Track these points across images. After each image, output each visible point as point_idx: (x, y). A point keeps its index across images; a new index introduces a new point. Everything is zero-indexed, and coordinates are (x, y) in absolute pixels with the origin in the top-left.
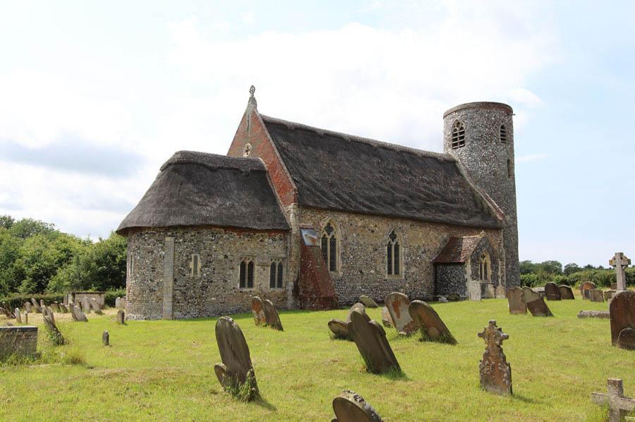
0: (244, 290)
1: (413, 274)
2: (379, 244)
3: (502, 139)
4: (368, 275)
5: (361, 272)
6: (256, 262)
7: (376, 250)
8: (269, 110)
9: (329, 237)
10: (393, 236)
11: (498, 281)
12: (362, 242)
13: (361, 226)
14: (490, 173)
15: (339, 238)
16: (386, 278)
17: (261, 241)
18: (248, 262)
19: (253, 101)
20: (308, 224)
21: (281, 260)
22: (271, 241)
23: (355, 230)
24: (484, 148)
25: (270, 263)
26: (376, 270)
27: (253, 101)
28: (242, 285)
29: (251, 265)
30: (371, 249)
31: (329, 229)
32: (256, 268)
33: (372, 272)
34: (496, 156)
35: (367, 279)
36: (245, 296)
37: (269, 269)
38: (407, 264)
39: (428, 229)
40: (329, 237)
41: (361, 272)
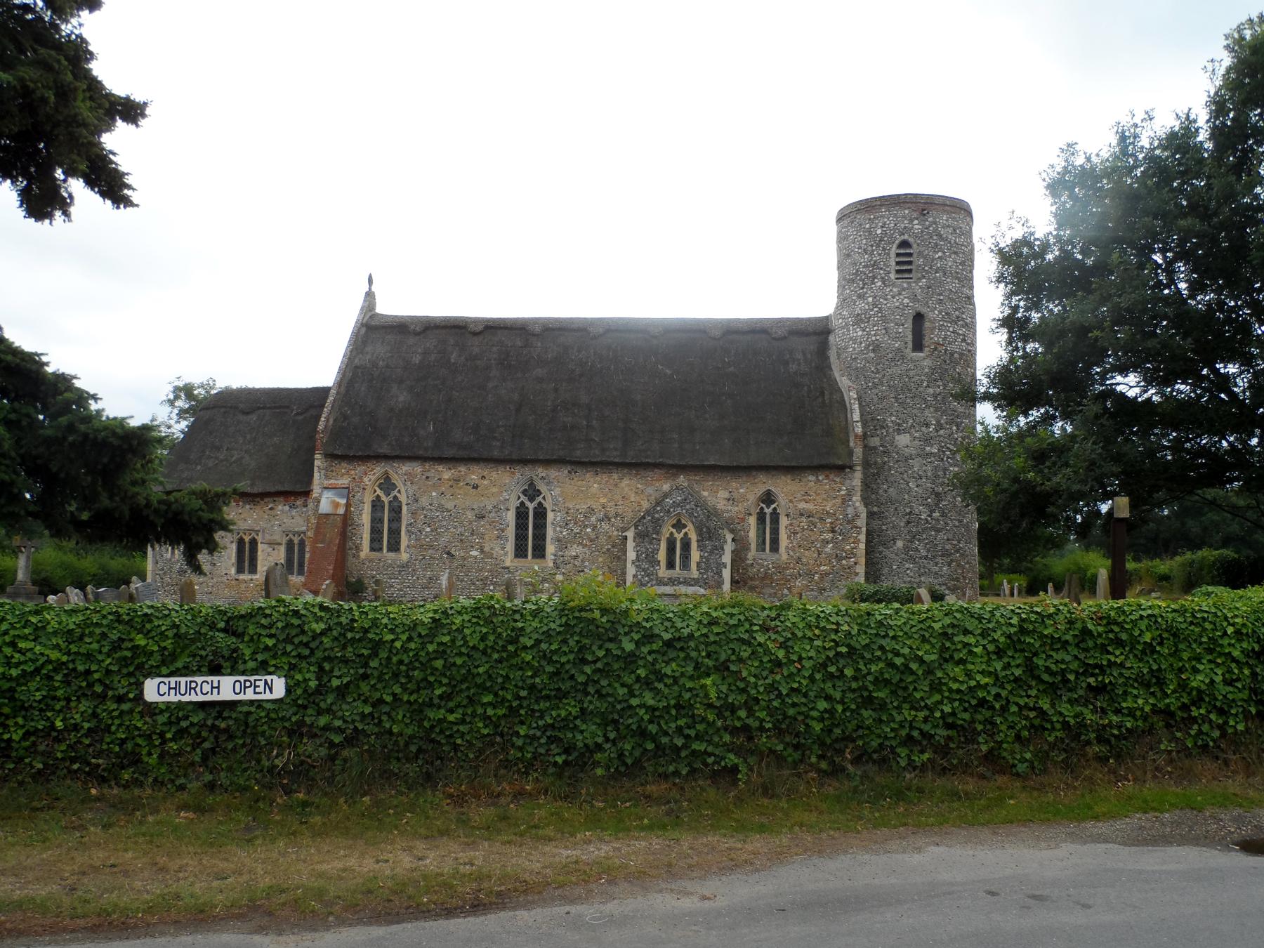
0: (242, 577)
1: (576, 557)
2: (489, 508)
3: (898, 272)
4: (464, 559)
5: (448, 553)
6: (259, 539)
7: (483, 517)
8: (391, 306)
9: (531, 506)
10: (532, 492)
11: (719, 573)
12: (450, 505)
13: (449, 480)
14: (867, 347)
15: (403, 498)
16: (508, 564)
17: (271, 509)
18: (247, 539)
19: (370, 296)
20: (340, 482)
21: (291, 536)
22: (287, 508)
23: (434, 487)
24: (859, 297)
25: (284, 541)
26: (482, 552)
27: (370, 296)
28: (240, 570)
29: (254, 543)
30: (470, 515)
31: (768, 498)
32: (260, 547)
33: (474, 553)
34: (880, 310)
35: (463, 566)
36: (243, 586)
37: (283, 549)
38: (559, 540)
39: (615, 476)
40: (531, 506)
41: (448, 553)
